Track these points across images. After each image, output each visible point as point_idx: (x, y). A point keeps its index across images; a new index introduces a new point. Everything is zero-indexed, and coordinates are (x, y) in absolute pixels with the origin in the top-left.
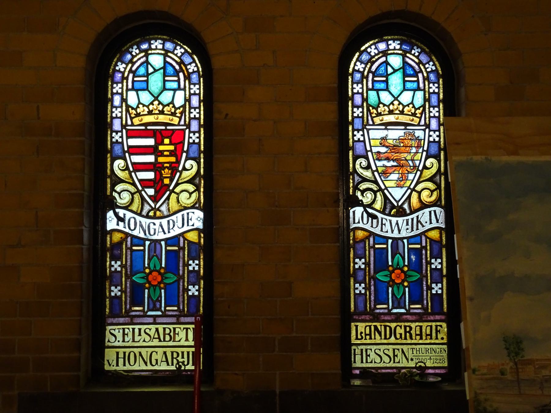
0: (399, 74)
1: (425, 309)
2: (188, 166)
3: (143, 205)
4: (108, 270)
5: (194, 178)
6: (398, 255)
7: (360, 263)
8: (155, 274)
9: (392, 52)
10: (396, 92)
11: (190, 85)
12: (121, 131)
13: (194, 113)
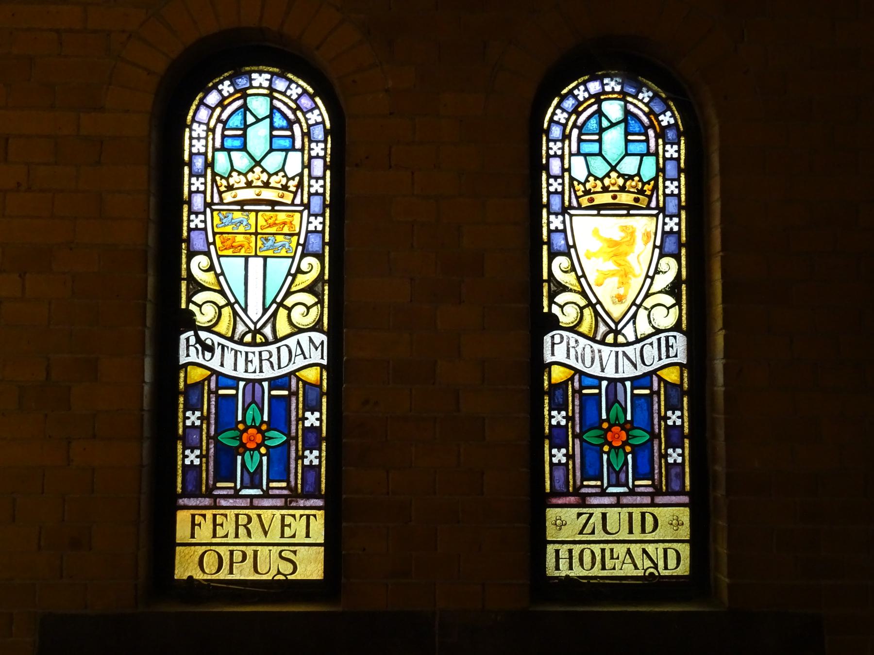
0: (619, 130)
1: (292, 489)
4: (181, 425)
6: (617, 405)
7: (193, 418)
10: (613, 158)
11: (664, 145)
12: (204, 213)
13: (317, 187)
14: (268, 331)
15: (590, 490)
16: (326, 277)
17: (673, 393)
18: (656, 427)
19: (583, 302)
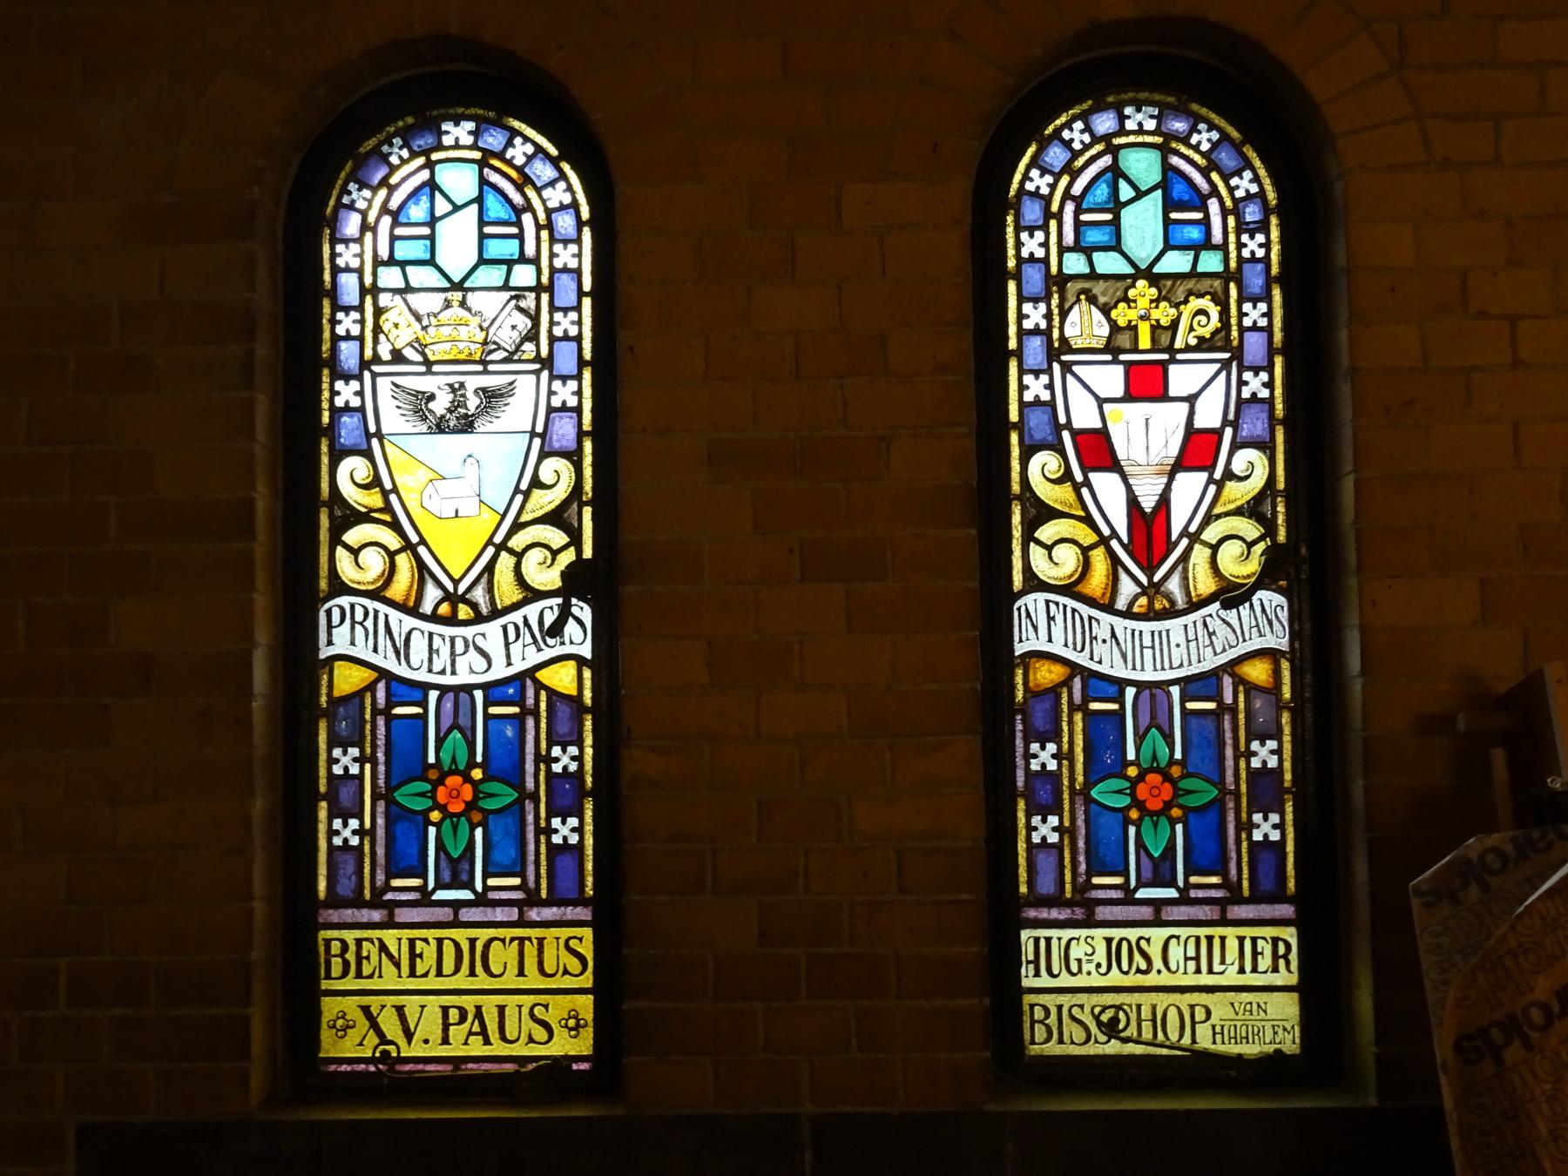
1: (1232, 888)
2: (1238, 467)
3: (1115, 580)
5: (1259, 498)
7: (1045, 757)
8: (1153, 778)
9: (1132, 139)
14: (1174, 585)
15: (1101, 894)
16: (1281, 485)
17: (563, 710)
18: (1229, 773)
19: (394, 542)
